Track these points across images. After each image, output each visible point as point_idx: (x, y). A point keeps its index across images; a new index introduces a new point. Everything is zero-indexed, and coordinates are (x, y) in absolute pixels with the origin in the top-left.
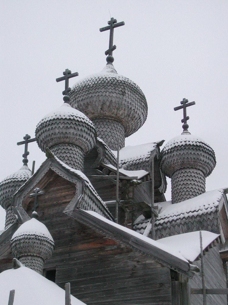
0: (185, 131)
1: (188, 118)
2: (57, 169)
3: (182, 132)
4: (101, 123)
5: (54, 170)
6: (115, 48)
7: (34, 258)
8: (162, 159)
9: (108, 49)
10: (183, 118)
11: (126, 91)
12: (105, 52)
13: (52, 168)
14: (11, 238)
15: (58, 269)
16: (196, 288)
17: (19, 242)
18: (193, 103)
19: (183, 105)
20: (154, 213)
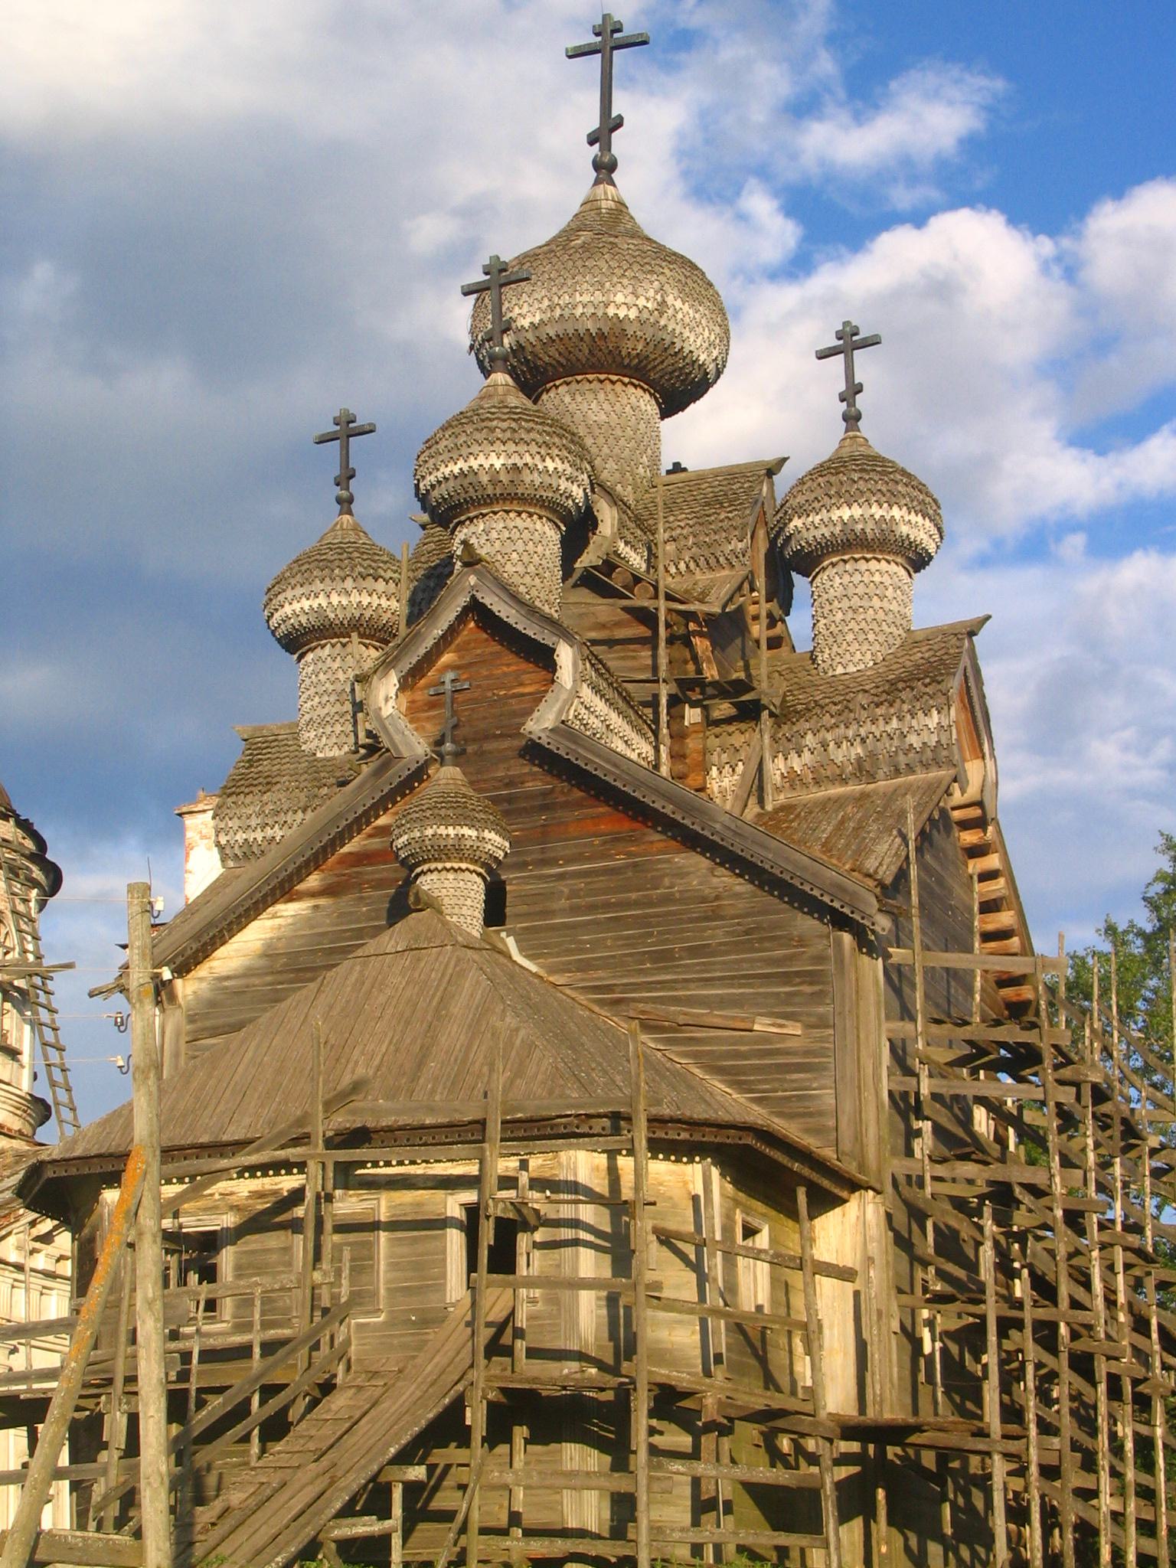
0: (851, 434)
1: (859, 389)
2: (497, 599)
3: (842, 435)
4: (590, 396)
5: (487, 601)
6: (619, 123)
7: (461, 876)
8: (787, 530)
9: (597, 125)
10: (842, 387)
11: (670, 300)
12: (589, 136)
13: (479, 596)
14: (969, 1352)
15: (514, 888)
16: (862, 565)
17: (418, 834)
18: (873, 342)
19: (841, 342)
20: (767, 708)
